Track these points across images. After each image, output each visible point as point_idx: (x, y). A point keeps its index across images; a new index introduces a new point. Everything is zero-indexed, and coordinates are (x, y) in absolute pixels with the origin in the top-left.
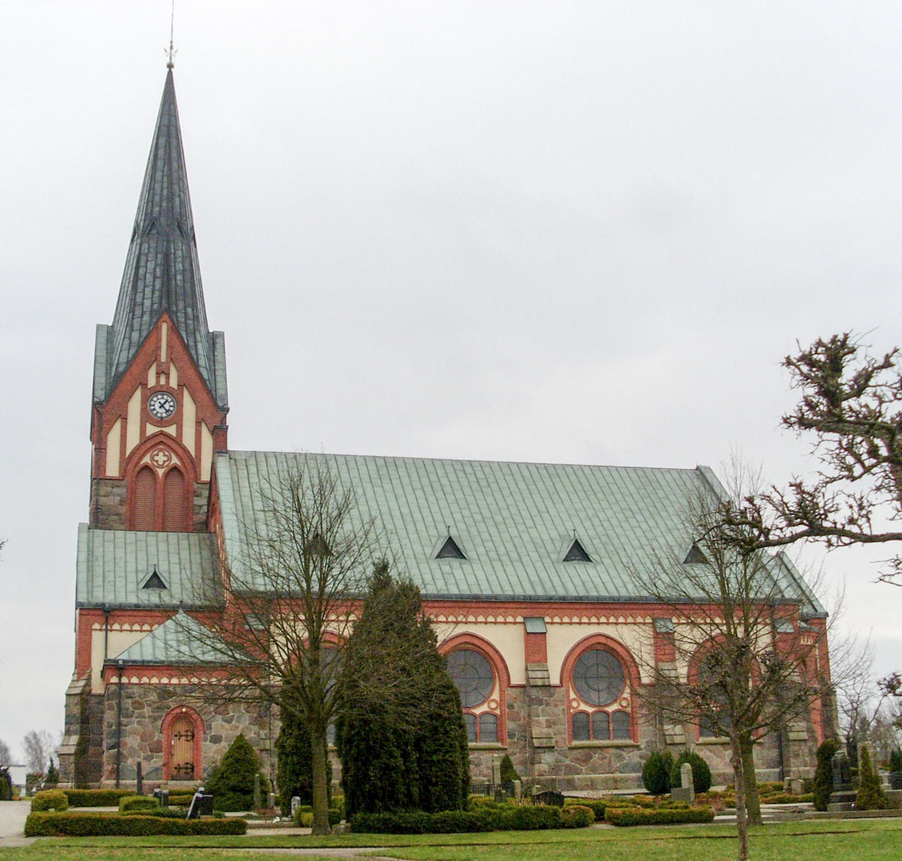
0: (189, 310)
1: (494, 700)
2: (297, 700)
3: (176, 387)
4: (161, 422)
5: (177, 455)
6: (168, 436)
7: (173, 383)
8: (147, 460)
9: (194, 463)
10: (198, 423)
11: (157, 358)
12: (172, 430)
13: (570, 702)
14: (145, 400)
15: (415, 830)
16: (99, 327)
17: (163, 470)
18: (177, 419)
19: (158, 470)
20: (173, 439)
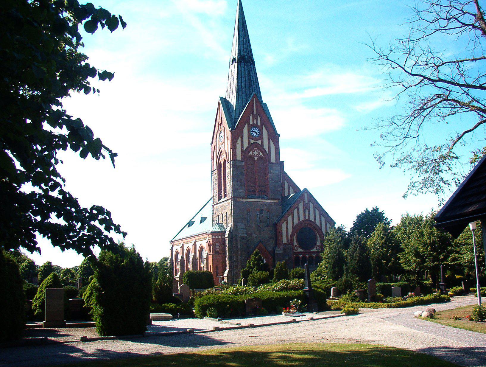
1: (318, 246)
7: (259, 124)
8: (251, 153)
11: (253, 112)
12: (259, 142)
13: (294, 247)
14: (250, 131)
15: (224, 353)
18: (261, 137)
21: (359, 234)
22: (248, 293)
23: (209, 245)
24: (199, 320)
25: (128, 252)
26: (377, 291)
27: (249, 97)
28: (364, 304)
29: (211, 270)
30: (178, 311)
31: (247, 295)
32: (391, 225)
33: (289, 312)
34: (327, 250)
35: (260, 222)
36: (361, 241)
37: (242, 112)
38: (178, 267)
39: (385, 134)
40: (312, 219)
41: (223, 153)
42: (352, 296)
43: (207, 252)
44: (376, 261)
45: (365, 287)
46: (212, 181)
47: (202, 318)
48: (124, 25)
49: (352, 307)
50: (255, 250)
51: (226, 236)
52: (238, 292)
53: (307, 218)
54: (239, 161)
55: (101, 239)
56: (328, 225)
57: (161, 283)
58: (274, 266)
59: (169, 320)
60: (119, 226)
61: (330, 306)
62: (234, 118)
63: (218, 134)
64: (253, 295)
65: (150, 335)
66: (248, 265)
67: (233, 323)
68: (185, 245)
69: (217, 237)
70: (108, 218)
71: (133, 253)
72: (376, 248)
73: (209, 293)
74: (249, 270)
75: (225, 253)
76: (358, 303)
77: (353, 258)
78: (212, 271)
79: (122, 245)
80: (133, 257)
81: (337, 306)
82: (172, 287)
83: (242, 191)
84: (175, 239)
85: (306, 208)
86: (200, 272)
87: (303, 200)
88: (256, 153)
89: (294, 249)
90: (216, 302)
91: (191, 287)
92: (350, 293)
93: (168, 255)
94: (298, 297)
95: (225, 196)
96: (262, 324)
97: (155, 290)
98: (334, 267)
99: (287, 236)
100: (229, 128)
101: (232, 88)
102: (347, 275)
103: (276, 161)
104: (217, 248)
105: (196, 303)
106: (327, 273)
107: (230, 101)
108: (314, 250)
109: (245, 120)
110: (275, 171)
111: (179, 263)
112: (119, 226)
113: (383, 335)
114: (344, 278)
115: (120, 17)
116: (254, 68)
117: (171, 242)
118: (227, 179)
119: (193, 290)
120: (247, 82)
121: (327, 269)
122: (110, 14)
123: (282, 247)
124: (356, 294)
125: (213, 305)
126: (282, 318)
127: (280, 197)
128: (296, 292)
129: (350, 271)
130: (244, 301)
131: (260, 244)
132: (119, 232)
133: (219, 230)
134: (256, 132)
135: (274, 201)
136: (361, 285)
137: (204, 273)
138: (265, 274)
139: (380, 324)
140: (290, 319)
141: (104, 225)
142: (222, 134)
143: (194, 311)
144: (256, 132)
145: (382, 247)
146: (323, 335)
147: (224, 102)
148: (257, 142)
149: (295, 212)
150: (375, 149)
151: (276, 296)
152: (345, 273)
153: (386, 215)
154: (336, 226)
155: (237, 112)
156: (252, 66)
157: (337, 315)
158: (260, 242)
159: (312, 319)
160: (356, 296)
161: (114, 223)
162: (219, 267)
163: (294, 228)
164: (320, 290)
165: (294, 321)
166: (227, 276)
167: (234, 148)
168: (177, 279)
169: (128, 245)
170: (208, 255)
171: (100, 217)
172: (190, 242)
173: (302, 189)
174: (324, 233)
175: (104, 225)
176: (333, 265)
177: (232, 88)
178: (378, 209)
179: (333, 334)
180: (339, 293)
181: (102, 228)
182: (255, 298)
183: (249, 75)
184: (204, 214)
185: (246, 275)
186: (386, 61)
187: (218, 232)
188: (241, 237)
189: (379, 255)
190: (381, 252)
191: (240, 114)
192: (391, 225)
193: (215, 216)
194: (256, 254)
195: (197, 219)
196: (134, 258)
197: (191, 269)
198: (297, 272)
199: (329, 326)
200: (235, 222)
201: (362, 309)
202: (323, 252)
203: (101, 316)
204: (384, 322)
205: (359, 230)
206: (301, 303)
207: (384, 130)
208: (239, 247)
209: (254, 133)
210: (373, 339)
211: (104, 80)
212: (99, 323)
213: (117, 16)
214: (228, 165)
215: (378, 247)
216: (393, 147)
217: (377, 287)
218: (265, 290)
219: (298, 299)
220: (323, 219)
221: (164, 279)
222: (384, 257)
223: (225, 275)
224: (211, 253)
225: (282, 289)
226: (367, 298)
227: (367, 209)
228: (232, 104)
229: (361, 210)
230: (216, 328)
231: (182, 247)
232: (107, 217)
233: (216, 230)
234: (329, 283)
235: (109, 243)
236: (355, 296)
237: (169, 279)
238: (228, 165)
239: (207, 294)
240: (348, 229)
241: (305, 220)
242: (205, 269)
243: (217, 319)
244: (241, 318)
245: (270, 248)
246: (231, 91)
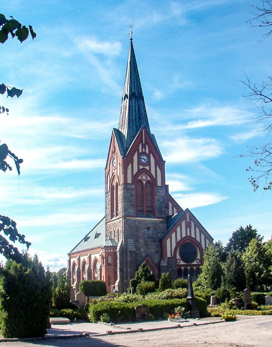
0: (139, 86)
1: (198, 259)
2: (140, 213)
3: (148, 153)
4: (143, 165)
5: (150, 177)
7: (147, 152)
8: (140, 178)
9: (155, 180)
11: (142, 142)
12: (147, 168)
14: (139, 158)
16: (18, 97)
18: (149, 163)
21: (235, 249)
22: (137, 301)
23: (103, 257)
24: (93, 324)
25: (31, 262)
26: (252, 299)
27: (139, 129)
28: (241, 311)
29: (104, 279)
30: (75, 316)
31: (137, 302)
32: (263, 241)
33: (174, 319)
34: (206, 263)
35: (148, 238)
36: (237, 255)
37: (132, 141)
38: (75, 277)
39: (258, 161)
40: (193, 236)
41: (116, 177)
42: (229, 304)
43: (100, 264)
44: (250, 273)
45: (242, 296)
46: (106, 202)
47: (96, 322)
48: (34, 35)
49: (230, 314)
50: (142, 262)
51: (118, 250)
52: (128, 300)
53: (188, 235)
54: (129, 184)
55: (6, 248)
56: (207, 241)
57: (60, 291)
58: (160, 276)
59: (67, 324)
60: (24, 236)
61: (210, 313)
62: (125, 147)
63: (112, 160)
64: (142, 302)
65: (50, 338)
66: (136, 276)
67: (124, 327)
68: (81, 258)
69: (109, 251)
70: (13, 229)
71: (36, 263)
72: (250, 262)
73: (103, 300)
74: (138, 280)
75: (116, 265)
76: (235, 311)
77: (230, 270)
78: (104, 281)
79: (26, 256)
80: (36, 266)
81: (217, 313)
82: (70, 294)
83: (132, 211)
84: (73, 252)
85: (188, 226)
86: (94, 282)
87: (186, 219)
88: (144, 177)
89: (177, 262)
90: (109, 308)
91: (86, 294)
92: (228, 302)
93: (66, 266)
94: (182, 305)
95: (117, 215)
96: (150, 328)
97: (55, 297)
98: (213, 278)
99: (171, 251)
100: (121, 155)
101: (124, 121)
102: (224, 285)
103: (162, 184)
104: (110, 261)
105: (91, 309)
106: (206, 283)
107: (122, 132)
108: (195, 263)
109: (135, 148)
110: (161, 193)
111: (76, 274)
112: (24, 236)
113: (261, 340)
114: (222, 288)
115: (31, 27)
116: (144, 103)
117: (69, 254)
118: (119, 199)
119: (88, 297)
120: (137, 117)
121: (206, 280)
122: (20, 25)
123: (166, 260)
124: (234, 302)
125: (106, 311)
126: (168, 323)
127: (165, 216)
128: (180, 300)
129: (227, 282)
130: (133, 308)
131: (20, 292)
132: (24, 242)
133: (112, 245)
134: (144, 159)
135: (160, 220)
136: (237, 295)
137: (97, 282)
138: (151, 284)
139: (257, 330)
140: (176, 324)
141: (9, 235)
142: (115, 161)
143: (89, 316)
144: (144, 159)
145: (255, 261)
146: (207, 340)
147: (117, 132)
148: (146, 167)
149: (178, 229)
150: (250, 173)
151: (162, 303)
152: (223, 283)
153: (258, 233)
154: (214, 242)
155: (129, 142)
156: (141, 101)
157: (217, 321)
158: (147, 256)
159: (195, 325)
160: (233, 305)
161: (19, 233)
162: (111, 278)
163: (177, 243)
164: (201, 298)
165: (179, 326)
166: (118, 285)
167: (125, 173)
168: (74, 287)
169: (31, 253)
170: (101, 267)
171: (6, 227)
172: (86, 255)
173: (184, 209)
174: (204, 248)
175: (9, 235)
176: (212, 277)
177: (124, 121)
178: (252, 227)
179: (215, 338)
180: (218, 302)
181: (7, 237)
182: (144, 305)
183: (139, 109)
184: (98, 230)
185: (135, 284)
186: (259, 97)
187: (111, 246)
188: (130, 252)
189: (253, 268)
190: (255, 265)
191: (131, 144)
192: (263, 241)
193: (108, 232)
194: (144, 266)
195: (92, 235)
196: (37, 267)
197: (87, 279)
198: (179, 283)
199: (211, 331)
200: (126, 237)
201: (239, 316)
202: (202, 265)
203: (5, 319)
204: (260, 328)
205: (235, 245)
206: (185, 310)
207: (258, 157)
208: (129, 260)
209: (143, 160)
210: (252, 344)
211: (12, 96)
212: (4, 326)
213: (28, 27)
214: (120, 188)
215: (252, 260)
216: (266, 172)
217: (252, 296)
218: (156, 298)
219: (182, 307)
220: (203, 237)
221: (63, 287)
222: (257, 269)
223: (117, 284)
224: (104, 265)
225: (167, 298)
226: (243, 306)
227: (241, 227)
228: (124, 134)
229: (236, 228)
230: (109, 332)
231: (79, 259)
232: (12, 227)
233: (109, 245)
234: (208, 293)
235: (14, 253)
236: (232, 305)
237: (67, 287)
238: (120, 188)
239: (98, 303)
240: (225, 245)
241: (187, 237)
242: (99, 279)
243: (110, 324)
244: (131, 323)
245: (156, 261)
246: (123, 123)
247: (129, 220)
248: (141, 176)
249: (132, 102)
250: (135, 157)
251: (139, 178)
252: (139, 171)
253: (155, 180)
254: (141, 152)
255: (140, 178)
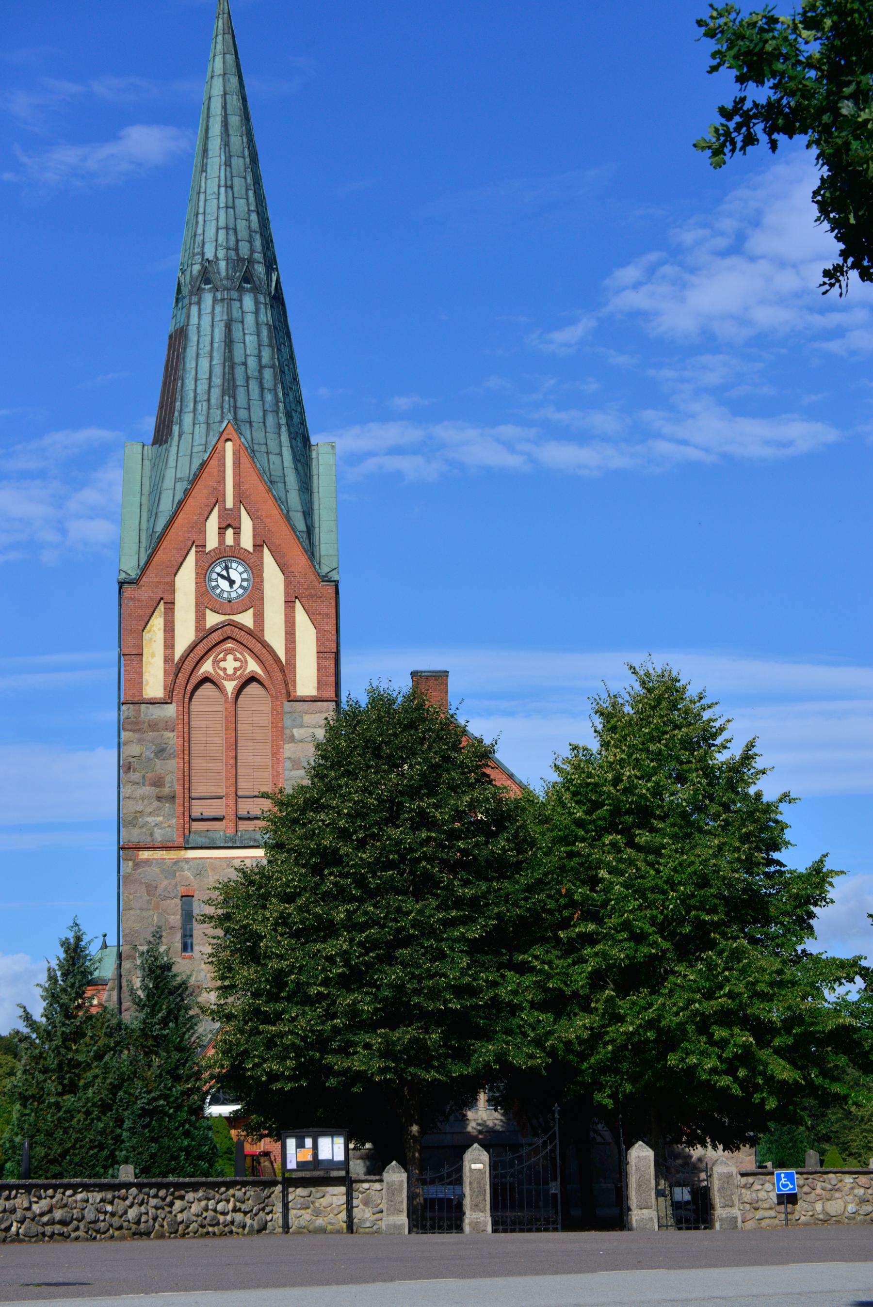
3: (251, 549)
6: (241, 628)
7: (247, 542)
8: (207, 667)
10: (289, 603)
11: (219, 500)
12: (246, 619)
17: (234, 683)
18: (254, 597)
19: (225, 683)
20: (249, 632)
54: (153, 702)
247: (147, 862)
248: (216, 657)
249: (200, 309)
250: (186, 580)
251: (202, 670)
252: (201, 635)
253: (282, 669)
254: (214, 550)
255: (211, 670)
